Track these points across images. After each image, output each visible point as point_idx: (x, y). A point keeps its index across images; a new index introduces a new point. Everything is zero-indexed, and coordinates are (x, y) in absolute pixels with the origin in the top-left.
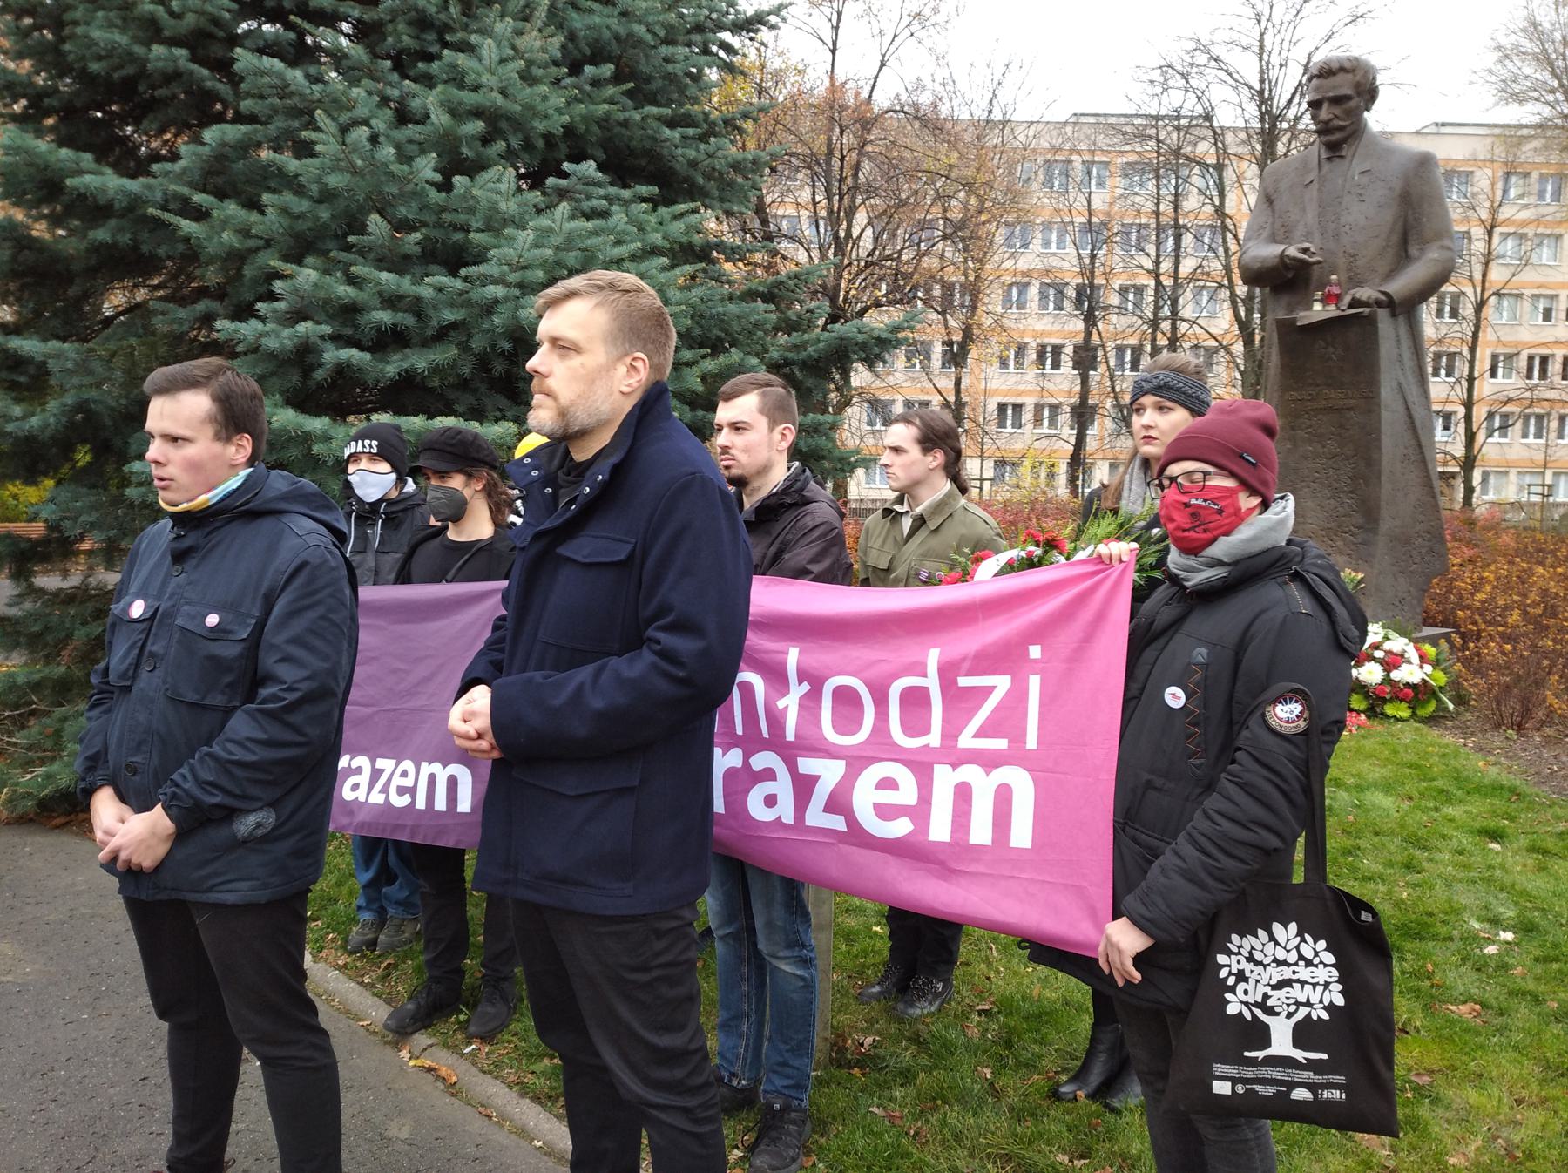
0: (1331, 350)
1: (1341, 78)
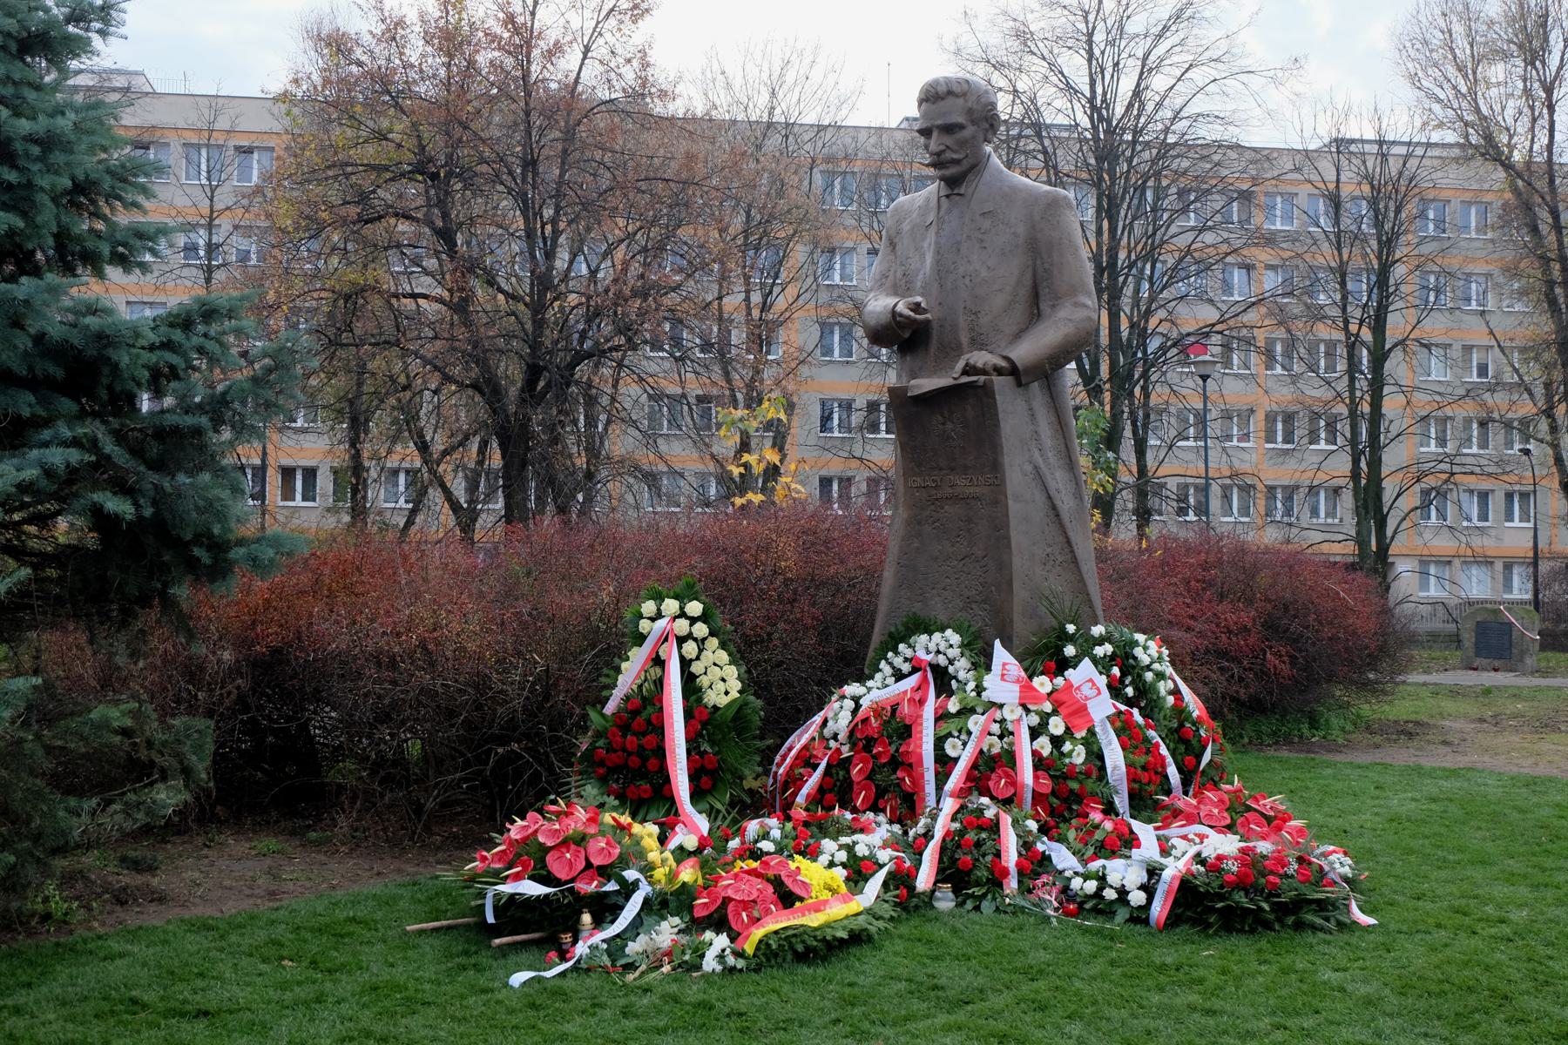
0: (949, 426)
1: (950, 100)
